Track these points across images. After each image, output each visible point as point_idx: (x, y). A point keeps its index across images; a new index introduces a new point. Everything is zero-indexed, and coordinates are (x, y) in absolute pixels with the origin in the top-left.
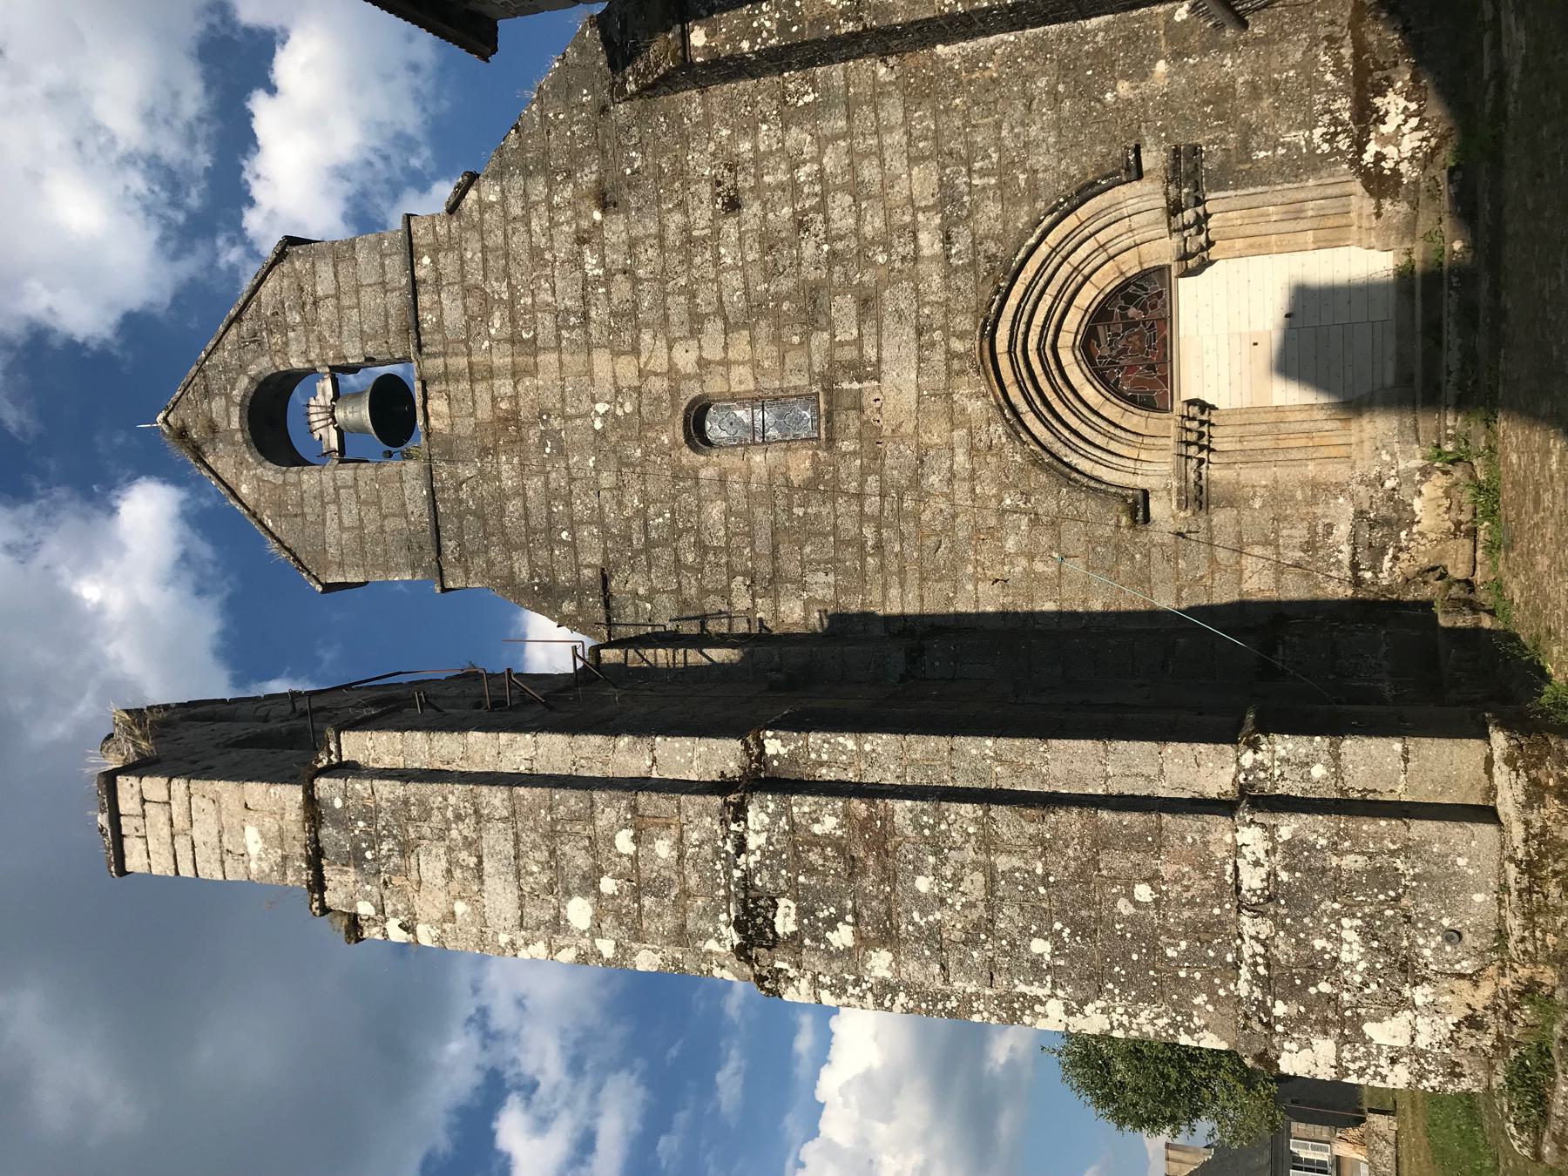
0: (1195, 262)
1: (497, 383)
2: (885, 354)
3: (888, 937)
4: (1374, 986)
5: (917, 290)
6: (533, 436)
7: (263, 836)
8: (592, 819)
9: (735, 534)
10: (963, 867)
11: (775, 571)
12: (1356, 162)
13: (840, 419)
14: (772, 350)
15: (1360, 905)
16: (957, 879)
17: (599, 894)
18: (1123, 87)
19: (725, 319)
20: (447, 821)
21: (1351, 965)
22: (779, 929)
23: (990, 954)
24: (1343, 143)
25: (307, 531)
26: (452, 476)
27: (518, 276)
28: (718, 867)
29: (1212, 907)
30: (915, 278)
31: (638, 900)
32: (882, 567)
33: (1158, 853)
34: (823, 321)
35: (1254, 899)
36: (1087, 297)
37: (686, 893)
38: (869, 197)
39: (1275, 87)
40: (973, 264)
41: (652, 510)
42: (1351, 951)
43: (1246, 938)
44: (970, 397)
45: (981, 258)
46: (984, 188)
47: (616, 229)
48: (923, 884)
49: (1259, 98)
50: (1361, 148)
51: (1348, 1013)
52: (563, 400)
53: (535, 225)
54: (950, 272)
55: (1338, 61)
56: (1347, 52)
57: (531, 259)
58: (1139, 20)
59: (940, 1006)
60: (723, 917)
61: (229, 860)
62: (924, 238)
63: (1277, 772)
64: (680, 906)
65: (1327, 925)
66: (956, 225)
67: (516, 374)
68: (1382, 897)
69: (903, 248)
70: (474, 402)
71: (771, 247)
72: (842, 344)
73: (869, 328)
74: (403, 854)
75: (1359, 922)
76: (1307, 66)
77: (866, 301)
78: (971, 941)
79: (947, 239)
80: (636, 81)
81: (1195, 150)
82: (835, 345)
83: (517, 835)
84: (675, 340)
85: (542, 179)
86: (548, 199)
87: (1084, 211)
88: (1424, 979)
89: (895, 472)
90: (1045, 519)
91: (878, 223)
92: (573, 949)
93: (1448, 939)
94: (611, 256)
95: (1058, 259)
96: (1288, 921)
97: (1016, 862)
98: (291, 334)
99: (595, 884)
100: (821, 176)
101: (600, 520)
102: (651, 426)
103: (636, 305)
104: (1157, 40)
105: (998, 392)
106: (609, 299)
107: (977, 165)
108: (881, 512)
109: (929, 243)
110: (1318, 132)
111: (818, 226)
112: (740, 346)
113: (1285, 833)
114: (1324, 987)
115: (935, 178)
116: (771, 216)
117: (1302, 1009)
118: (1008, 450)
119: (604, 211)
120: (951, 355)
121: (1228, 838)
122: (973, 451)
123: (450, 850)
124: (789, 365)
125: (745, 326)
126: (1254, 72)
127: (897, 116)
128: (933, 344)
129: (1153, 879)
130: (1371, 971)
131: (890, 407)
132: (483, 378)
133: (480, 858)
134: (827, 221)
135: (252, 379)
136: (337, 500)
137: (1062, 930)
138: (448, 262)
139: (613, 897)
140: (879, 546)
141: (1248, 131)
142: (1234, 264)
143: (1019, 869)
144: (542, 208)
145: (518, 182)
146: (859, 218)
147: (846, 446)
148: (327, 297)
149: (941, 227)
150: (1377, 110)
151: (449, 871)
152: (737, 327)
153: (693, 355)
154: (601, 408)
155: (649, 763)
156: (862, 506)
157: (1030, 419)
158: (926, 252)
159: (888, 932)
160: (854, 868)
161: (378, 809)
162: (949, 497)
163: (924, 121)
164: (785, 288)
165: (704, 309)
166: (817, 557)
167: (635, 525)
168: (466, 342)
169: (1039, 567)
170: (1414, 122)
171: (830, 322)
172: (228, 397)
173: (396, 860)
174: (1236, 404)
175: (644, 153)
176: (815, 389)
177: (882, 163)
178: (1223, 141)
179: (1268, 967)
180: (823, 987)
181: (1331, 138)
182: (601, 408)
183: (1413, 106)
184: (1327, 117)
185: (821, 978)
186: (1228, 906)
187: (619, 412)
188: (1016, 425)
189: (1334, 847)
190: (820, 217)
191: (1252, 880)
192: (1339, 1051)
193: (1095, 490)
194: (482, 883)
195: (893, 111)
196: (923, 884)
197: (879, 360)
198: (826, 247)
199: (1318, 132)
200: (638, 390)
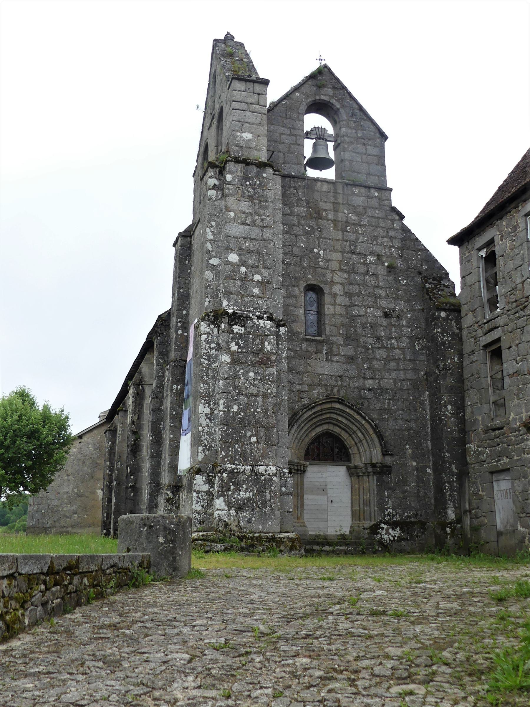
0: (353, 472)
1: (332, 213)
2: (334, 364)
3: (234, 362)
5: (354, 377)
6: (312, 223)
7: (249, 140)
8: (264, 268)
12: (381, 522)
13: (313, 344)
14: (338, 322)
15: (256, 498)
16: (254, 385)
18: (410, 451)
19: (350, 306)
21: (239, 495)
22: (234, 327)
24: (387, 518)
25: (280, 118)
26: (299, 186)
27: (369, 229)
30: (358, 377)
31: (239, 279)
34: (347, 342)
36: (344, 435)
38: (385, 364)
39: (405, 498)
40: (361, 397)
44: (318, 392)
45: (363, 400)
46: (384, 403)
47: (382, 270)
48: (251, 374)
49: (402, 493)
52: (325, 238)
53: (386, 240)
54: (360, 389)
55: (410, 517)
56: (413, 519)
57: (375, 236)
58: (429, 457)
61: (239, 124)
62: (371, 381)
64: (238, 294)
66: (374, 393)
67: (335, 221)
69: (368, 374)
70: (326, 202)
71: (372, 327)
72: (339, 348)
73: (343, 359)
74: (249, 197)
76: (410, 508)
77: (352, 359)
79: (370, 390)
80: (429, 288)
81: (390, 473)
84: (344, 286)
85: (400, 245)
87: (374, 436)
91: (377, 366)
93: (250, 519)
94: (373, 266)
95: (359, 426)
97: (260, 403)
98: (354, 131)
100: (393, 348)
102: (315, 271)
103: (356, 273)
104: (422, 463)
109: (369, 383)
110: (391, 511)
112: (340, 310)
113: (275, 479)
114: (232, 487)
115: (389, 387)
116: (382, 328)
118: (300, 404)
119: (388, 267)
120: (332, 387)
121: (271, 464)
122: (300, 392)
123: (251, 214)
124: (333, 328)
125: (347, 313)
126: (410, 492)
127: (409, 377)
128: (336, 381)
129: (258, 442)
130: (238, 500)
132: (334, 208)
133: (249, 225)
134: (379, 348)
135: (338, 109)
136: (291, 135)
139: (239, 271)
141: (393, 489)
142: (349, 484)
144: (390, 244)
145: (400, 236)
146: (378, 360)
147: (304, 345)
148: (366, 149)
149: (374, 388)
151: (244, 213)
152: (347, 310)
153: (338, 292)
154: (322, 253)
157: (310, 413)
158: (366, 382)
159: (236, 362)
160: (256, 353)
161: (263, 190)
163: (407, 385)
165: (354, 299)
168: (347, 203)
170: (392, 538)
171: (346, 345)
172: (332, 97)
173: (247, 193)
174: (305, 483)
175: (405, 285)
177: (395, 370)
178: (391, 481)
179: (237, 472)
180: (208, 336)
181: (389, 515)
182: (322, 253)
183: (396, 538)
187: (320, 260)
188: (308, 407)
189: (272, 491)
192: (204, 492)
195: (410, 375)
196: (251, 374)
197: (332, 361)
199: (391, 511)
200: (327, 268)
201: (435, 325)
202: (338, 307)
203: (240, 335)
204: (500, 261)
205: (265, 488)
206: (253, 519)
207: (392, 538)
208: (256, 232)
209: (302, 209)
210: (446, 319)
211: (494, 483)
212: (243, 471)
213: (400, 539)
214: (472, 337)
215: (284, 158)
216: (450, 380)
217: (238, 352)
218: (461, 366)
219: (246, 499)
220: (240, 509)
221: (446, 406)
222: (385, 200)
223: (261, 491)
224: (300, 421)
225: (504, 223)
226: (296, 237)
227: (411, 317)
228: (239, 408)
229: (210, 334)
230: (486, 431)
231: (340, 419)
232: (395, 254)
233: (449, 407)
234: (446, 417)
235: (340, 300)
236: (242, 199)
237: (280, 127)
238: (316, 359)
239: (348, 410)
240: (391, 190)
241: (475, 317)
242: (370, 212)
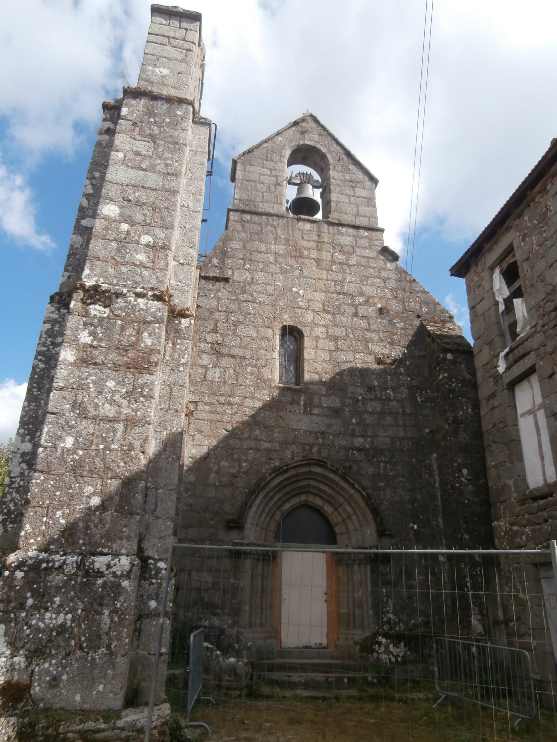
2: (314, 417)
4: (28, 632)
5: (340, 434)
6: (292, 261)
9: (241, 339)
10: (119, 406)
11: (222, 355)
12: (377, 634)
15: (79, 626)
16: (112, 402)
17: (120, 222)
19: (335, 351)
20: (166, 159)
21: (42, 619)
22: (92, 307)
23: (67, 414)
24: (386, 627)
28: (129, 282)
29: (84, 539)
31: (115, 240)
32: (220, 404)
33: (118, 512)
35: (87, 564)
36: (328, 509)
37: (117, 264)
41: (255, 305)
42: (51, 618)
43: (64, 558)
44: (293, 452)
48: (111, 384)
50: (385, 636)
51: (12, 615)
52: (307, 278)
54: (347, 449)
59: (35, 385)
60: (101, 280)
62: (361, 440)
63: (154, 581)
65: (69, 606)
67: (318, 261)
68: (83, 638)
69: (358, 430)
70: (308, 241)
71: (362, 375)
72: (320, 399)
74: (151, 136)
75: (69, 625)
78: (75, 405)
79: (359, 450)
82: (320, 395)
83: (155, 190)
86: (387, 288)
87: (367, 511)
88: (30, 663)
89: (262, 415)
90: (234, 481)
91: (368, 421)
92: (87, 206)
93: (54, 679)
96: (73, 582)
98: (341, 174)
99: (125, 221)
101: (253, 282)
105: (295, 465)
106: (346, 304)
107: (388, 466)
108: (245, 406)
110: (391, 616)
111: (369, 396)
113: (125, 583)
114: (30, 602)
116: (374, 377)
117: (18, 588)
118: (267, 467)
120: (312, 445)
122: (269, 451)
123: (151, 157)
131: (291, 417)
133: (145, 170)
137: (77, 454)
138: (365, 242)
139: (118, 229)
140: (229, 404)
143: (115, 435)
148: (355, 192)
150: (399, 643)
152: (331, 355)
155: (181, 262)
156: (249, 398)
157: (281, 478)
158: (355, 440)
160: (123, 349)
162: (249, 438)
164: (345, 378)
165: (340, 343)
166: (227, 375)
167: (250, 298)
169: (212, 476)
170: (393, 659)
176: (302, 385)
177: (392, 426)
179: (46, 569)
180: (53, 326)
181: (389, 622)
182: (301, 292)
183: (400, 659)
184: (397, 620)
185: (58, 325)
186: (84, 548)
187: (299, 299)
188: (278, 471)
189: (115, 611)
190: (372, 397)
191: (100, 562)
193: (246, 505)
194: (132, 168)
196: (111, 384)
197: (312, 414)
198: (360, 398)
199: (391, 616)
201: (439, 370)
202: (319, 352)
203: (101, 319)
204: (524, 269)
205: (101, 605)
206: (65, 677)
207: (393, 659)
208: (153, 180)
209: (280, 247)
210: (454, 362)
211: (543, 581)
212: (61, 567)
213: (405, 662)
214: (490, 377)
215: (263, 197)
216: (463, 437)
217: (91, 346)
218: (478, 418)
219: (55, 628)
220: (37, 653)
221: (460, 471)
222: (376, 240)
223: (91, 612)
224: (267, 490)
225: (526, 218)
226: (272, 275)
227: (411, 364)
228: (76, 441)
229: (59, 322)
230: (522, 502)
231: (322, 487)
232: (389, 296)
233: (465, 471)
234: (461, 484)
235: (323, 343)
236: (138, 137)
237: (259, 168)
238: (291, 411)
239: (332, 476)
240: (382, 230)
241: (491, 349)
242: (359, 252)
